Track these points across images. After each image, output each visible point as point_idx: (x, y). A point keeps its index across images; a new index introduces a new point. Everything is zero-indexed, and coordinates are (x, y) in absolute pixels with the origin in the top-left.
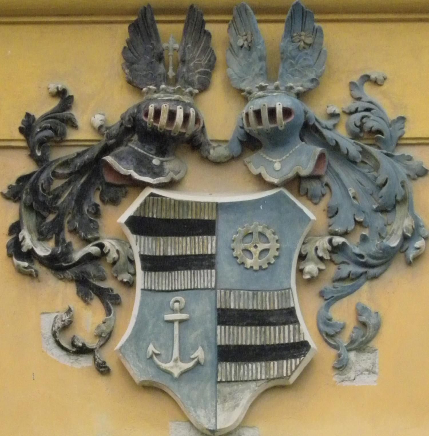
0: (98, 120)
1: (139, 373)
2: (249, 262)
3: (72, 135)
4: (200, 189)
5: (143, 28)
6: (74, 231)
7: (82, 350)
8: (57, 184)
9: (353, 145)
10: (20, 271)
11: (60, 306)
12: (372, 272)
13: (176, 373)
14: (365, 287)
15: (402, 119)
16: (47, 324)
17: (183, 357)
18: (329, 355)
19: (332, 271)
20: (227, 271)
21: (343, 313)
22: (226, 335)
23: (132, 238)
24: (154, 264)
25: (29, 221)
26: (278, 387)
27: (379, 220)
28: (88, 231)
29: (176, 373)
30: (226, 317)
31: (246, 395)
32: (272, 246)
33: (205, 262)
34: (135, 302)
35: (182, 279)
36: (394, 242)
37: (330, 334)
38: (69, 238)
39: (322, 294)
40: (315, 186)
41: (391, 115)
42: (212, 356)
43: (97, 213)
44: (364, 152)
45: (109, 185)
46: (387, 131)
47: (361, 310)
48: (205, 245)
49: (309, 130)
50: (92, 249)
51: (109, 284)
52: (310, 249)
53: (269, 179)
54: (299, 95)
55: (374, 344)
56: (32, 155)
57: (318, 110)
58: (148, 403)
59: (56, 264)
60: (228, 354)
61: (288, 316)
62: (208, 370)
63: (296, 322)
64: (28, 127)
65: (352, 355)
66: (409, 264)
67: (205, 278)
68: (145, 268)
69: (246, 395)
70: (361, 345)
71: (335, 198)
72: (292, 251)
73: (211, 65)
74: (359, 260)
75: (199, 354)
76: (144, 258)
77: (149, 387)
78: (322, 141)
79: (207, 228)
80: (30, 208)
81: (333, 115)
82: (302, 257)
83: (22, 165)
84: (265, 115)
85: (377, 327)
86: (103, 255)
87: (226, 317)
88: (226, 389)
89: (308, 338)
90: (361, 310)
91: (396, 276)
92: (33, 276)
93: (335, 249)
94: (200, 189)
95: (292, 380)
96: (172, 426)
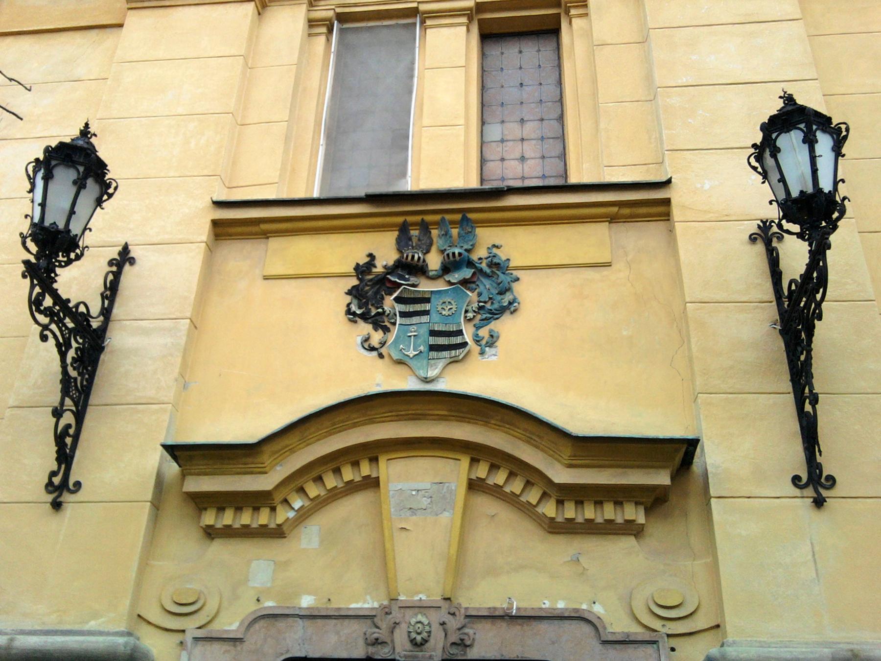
0: (385, 263)
1: (396, 356)
2: (444, 313)
3: (374, 270)
4: (425, 286)
5: (404, 229)
6: (372, 305)
7: (372, 349)
8: (367, 288)
9: (287, 564)
10: (350, 320)
11: (365, 333)
12: (496, 316)
13: (411, 356)
14: (493, 322)
15: (508, 260)
16: (359, 340)
17: (414, 350)
18: (476, 349)
19: (479, 317)
20: (435, 317)
21: (484, 332)
22: (433, 341)
23: (396, 305)
24: (403, 315)
25: (355, 302)
26: (455, 361)
27: (499, 297)
28: (379, 303)
29: (411, 356)
30: (433, 333)
31: (441, 364)
32: (454, 307)
33: (426, 313)
34: (395, 330)
35: (415, 320)
36: (505, 304)
37: (477, 341)
38: (370, 307)
39: (474, 326)
40: (473, 286)
41: (504, 258)
42: (427, 349)
43: (383, 298)
44: (492, 272)
45: (388, 288)
46: (502, 265)
47: (491, 331)
48: (427, 307)
49: (470, 264)
50: (380, 310)
51: (387, 324)
52: (470, 308)
53: (453, 281)
54: (466, 250)
55: (496, 344)
56: (358, 278)
57: (474, 257)
58: (400, 368)
59: (365, 317)
60: (433, 348)
61: (460, 333)
62: (425, 354)
63: (463, 334)
64: (357, 268)
65: (487, 349)
66: (512, 313)
67: (425, 319)
68: (400, 316)
69: (441, 364)
70: (491, 345)
71: (482, 288)
72: (461, 309)
73: (431, 244)
74: (490, 312)
75: (422, 348)
76: (400, 312)
77: (400, 362)
78: (476, 267)
79: (428, 300)
80: (355, 297)
81: (480, 259)
82: (466, 311)
83: (355, 282)
84: (451, 255)
85: (498, 337)
86: (384, 312)
87: (433, 333)
88: (432, 362)
89: (467, 340)
90: (491, 331)
91: (506, 318)
92: (356, 322)
93: (480, 308)
94: (425, 286)
95: (461, 357)
96: (409, 377)
